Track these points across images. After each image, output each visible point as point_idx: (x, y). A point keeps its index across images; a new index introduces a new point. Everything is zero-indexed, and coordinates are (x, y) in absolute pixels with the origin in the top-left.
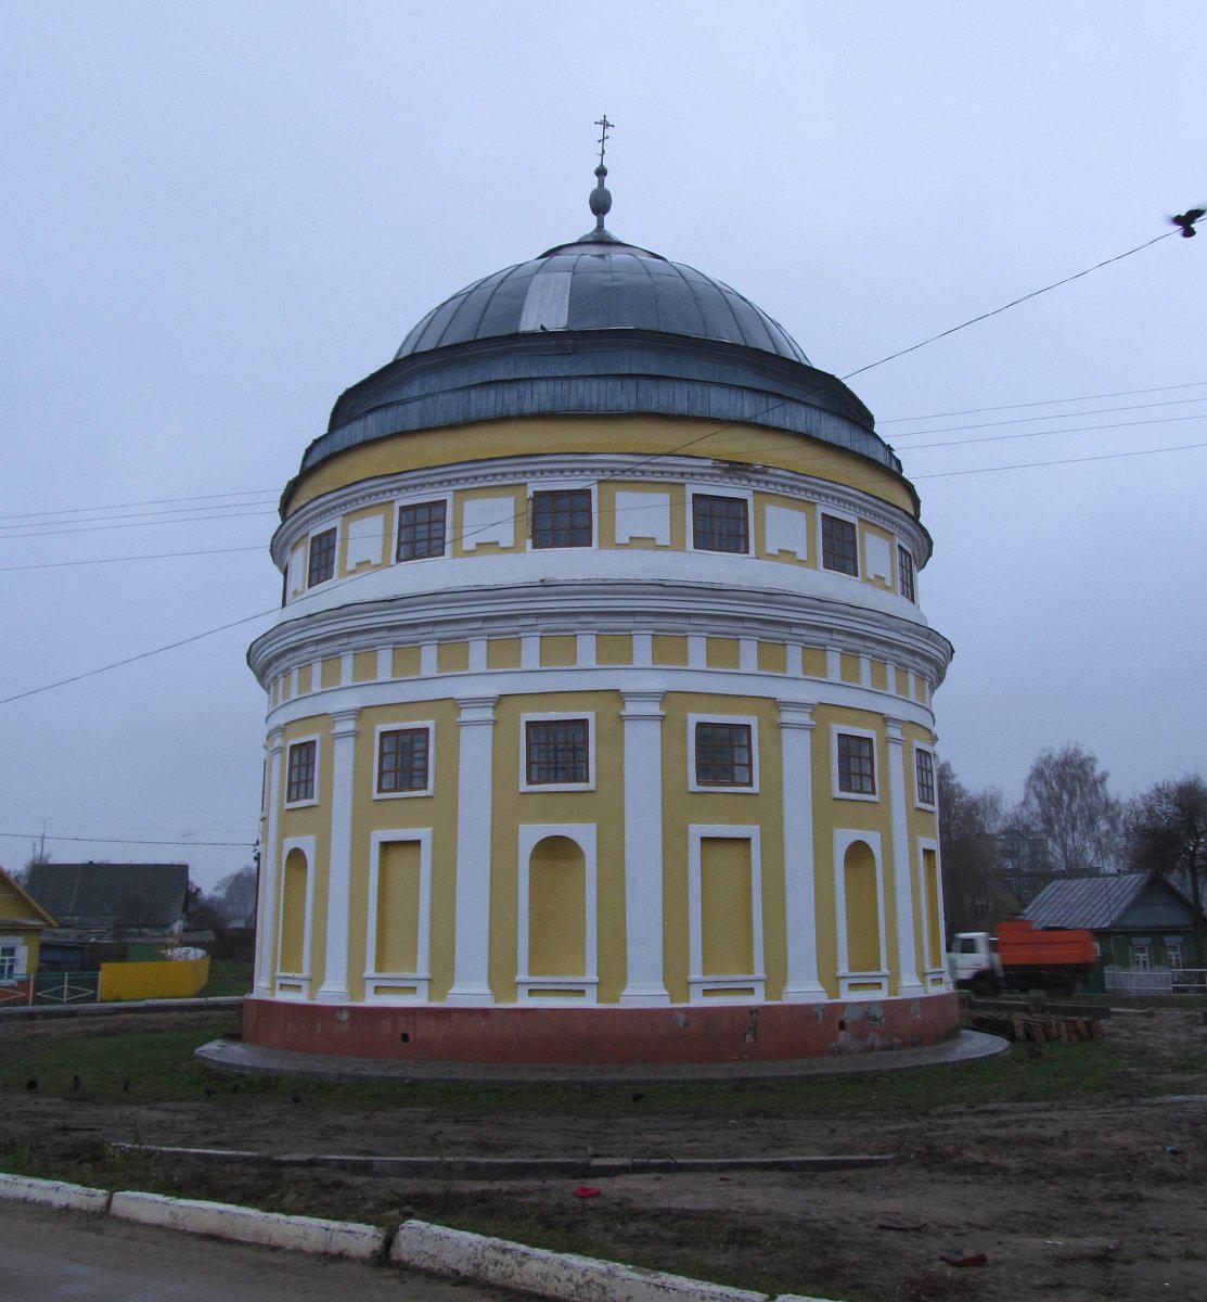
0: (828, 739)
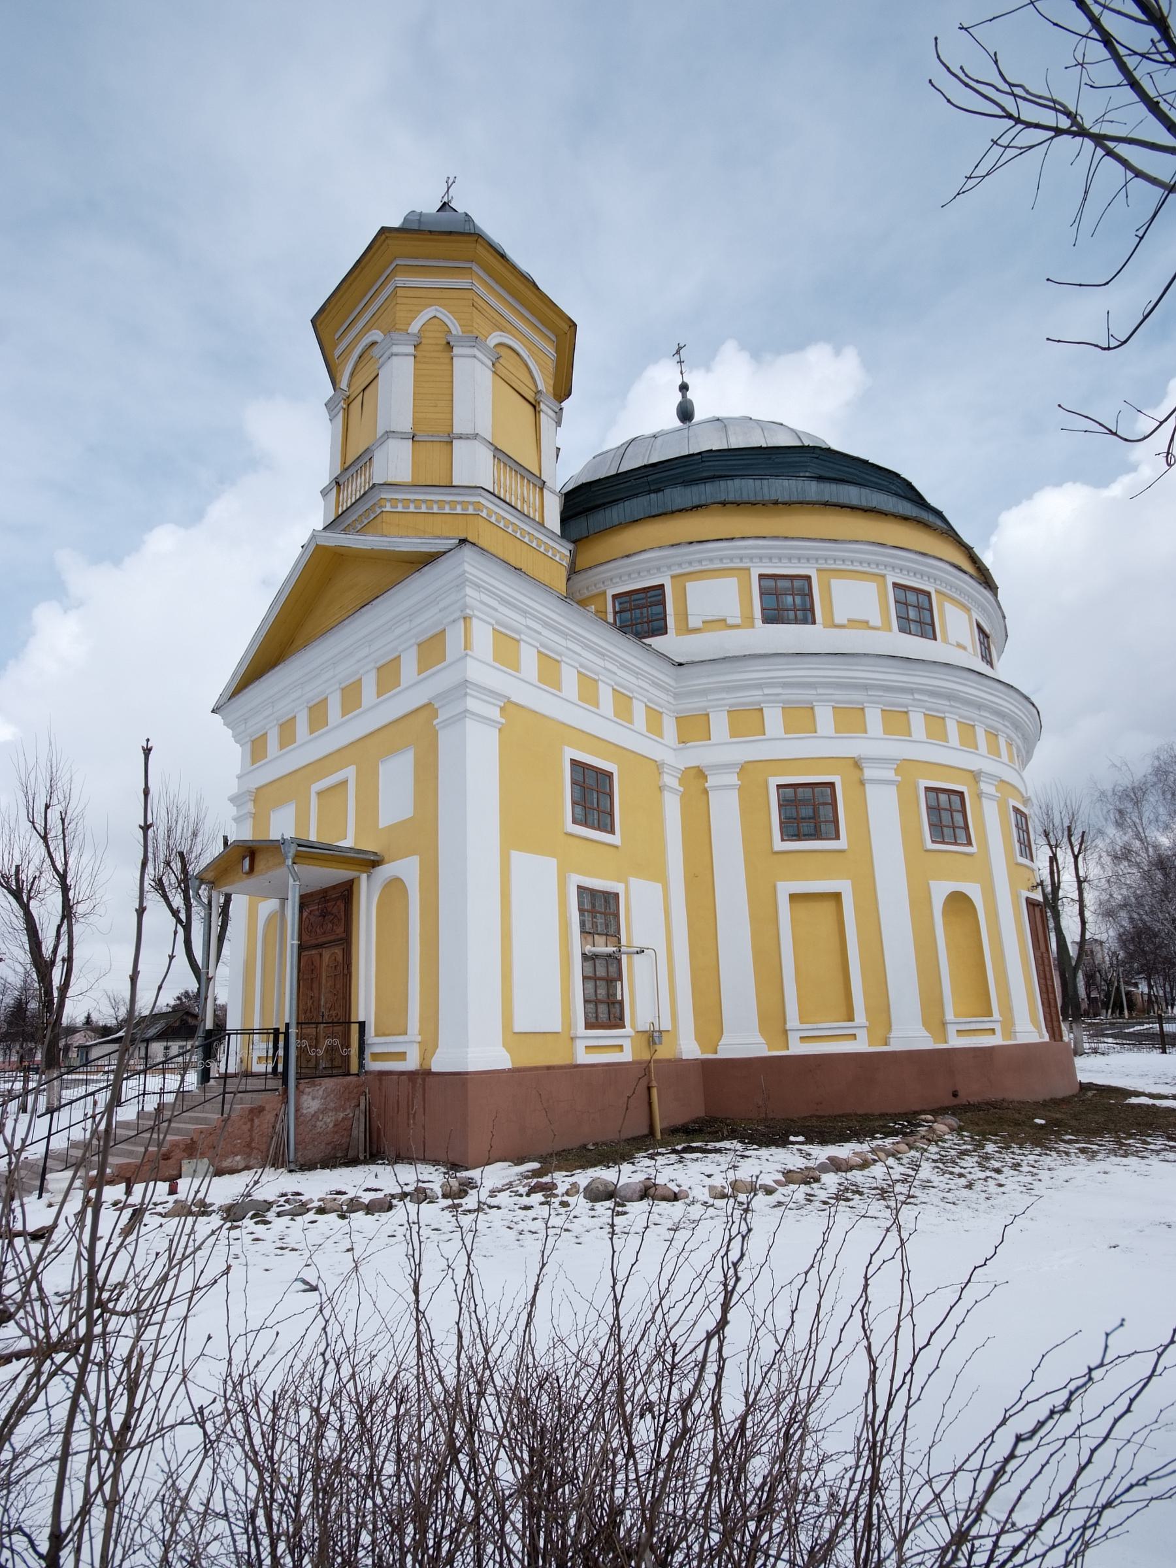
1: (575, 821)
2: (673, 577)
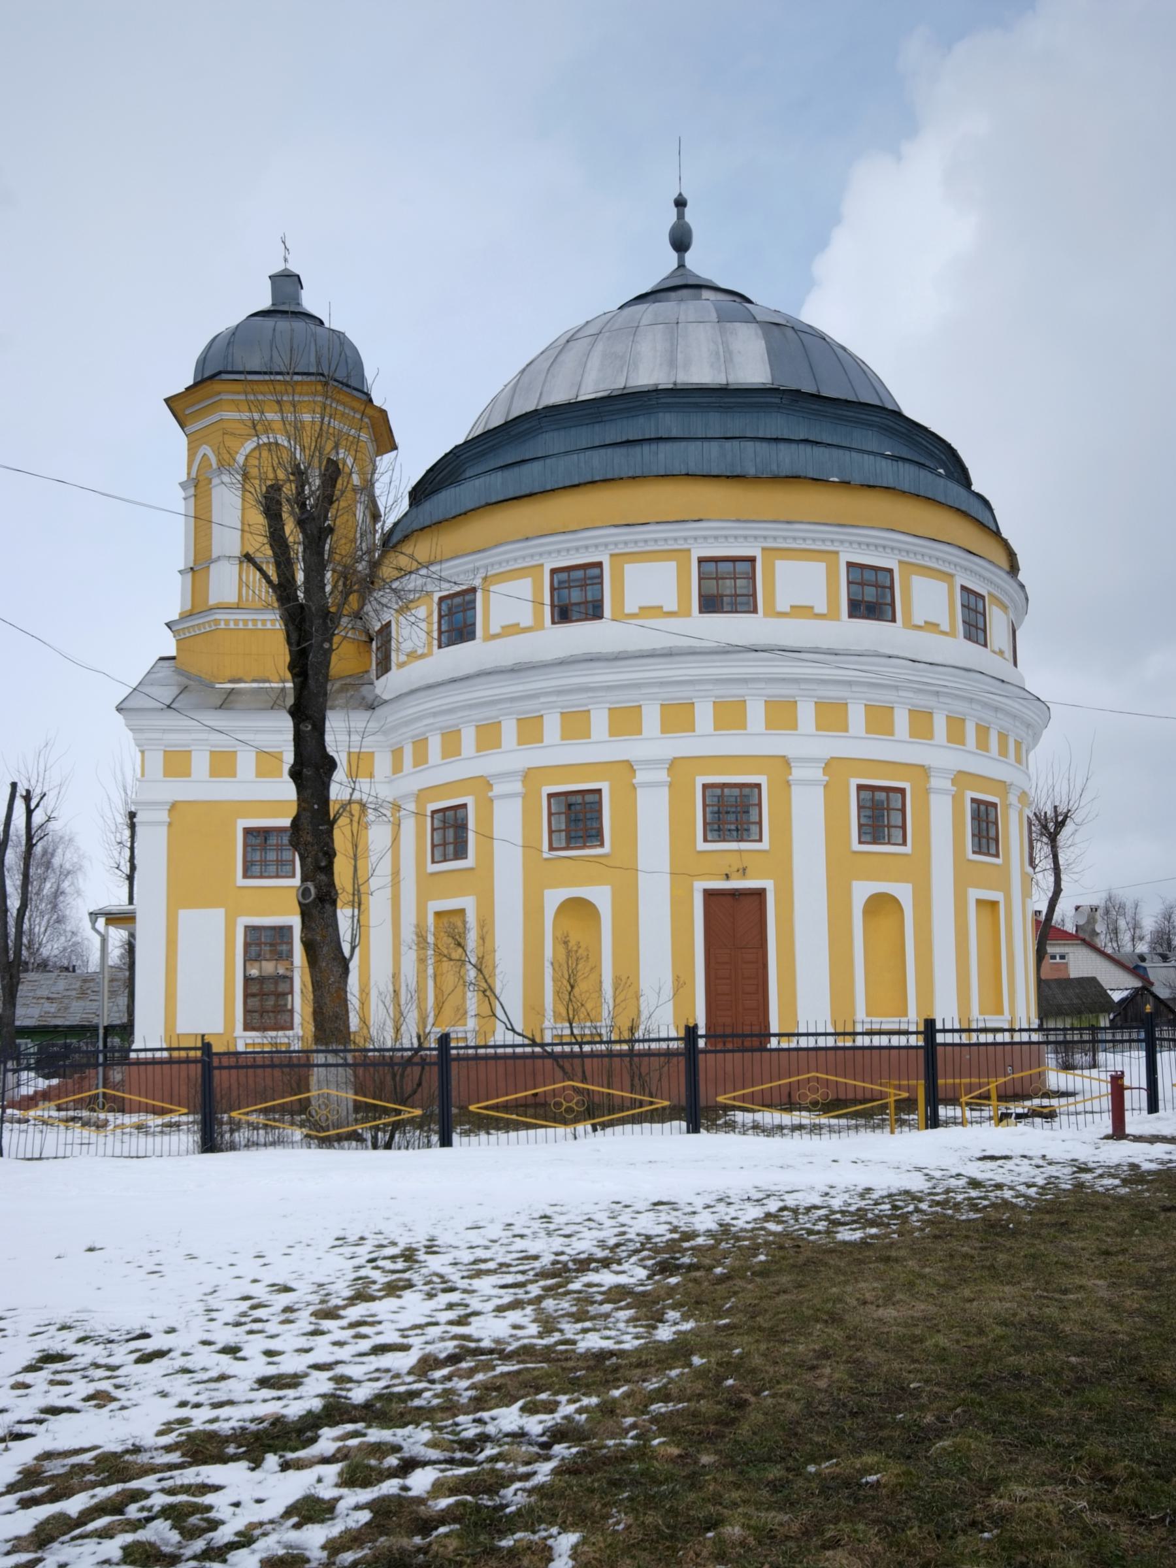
0: (541, 797)
1: (974, 852)
2: (612, 555)
